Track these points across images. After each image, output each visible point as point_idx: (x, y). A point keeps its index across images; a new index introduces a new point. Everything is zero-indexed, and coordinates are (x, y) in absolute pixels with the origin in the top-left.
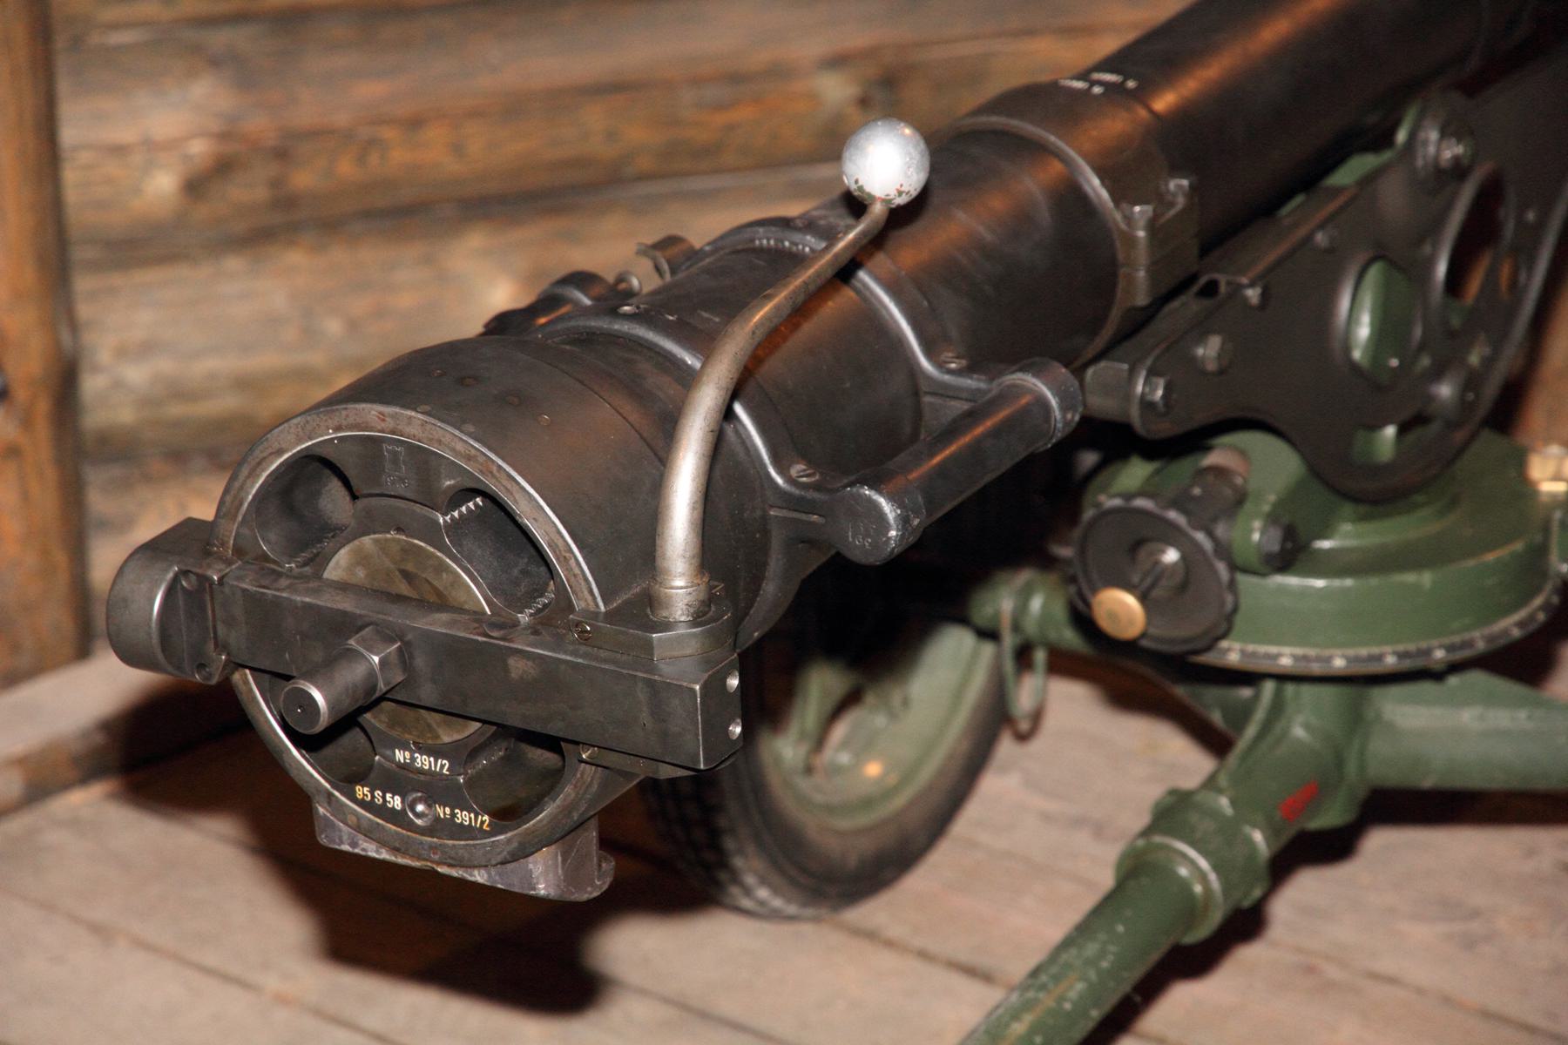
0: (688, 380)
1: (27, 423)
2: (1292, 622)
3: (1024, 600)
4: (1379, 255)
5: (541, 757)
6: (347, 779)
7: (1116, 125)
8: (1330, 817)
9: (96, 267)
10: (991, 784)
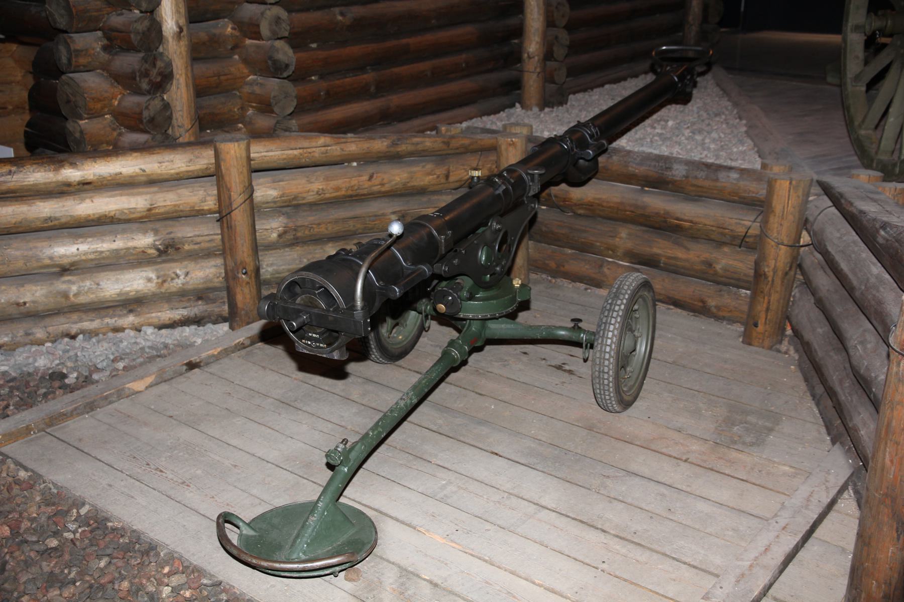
0: (360, 266)
1: (250, 278)
2: (473, 310)
3: (424, 305)
4: (486, 244)
5: (335, 334)
6: (301, 339)
7: (439, 222)
8: (479, 344)
9: (263, 250)
10: (421, 339)
